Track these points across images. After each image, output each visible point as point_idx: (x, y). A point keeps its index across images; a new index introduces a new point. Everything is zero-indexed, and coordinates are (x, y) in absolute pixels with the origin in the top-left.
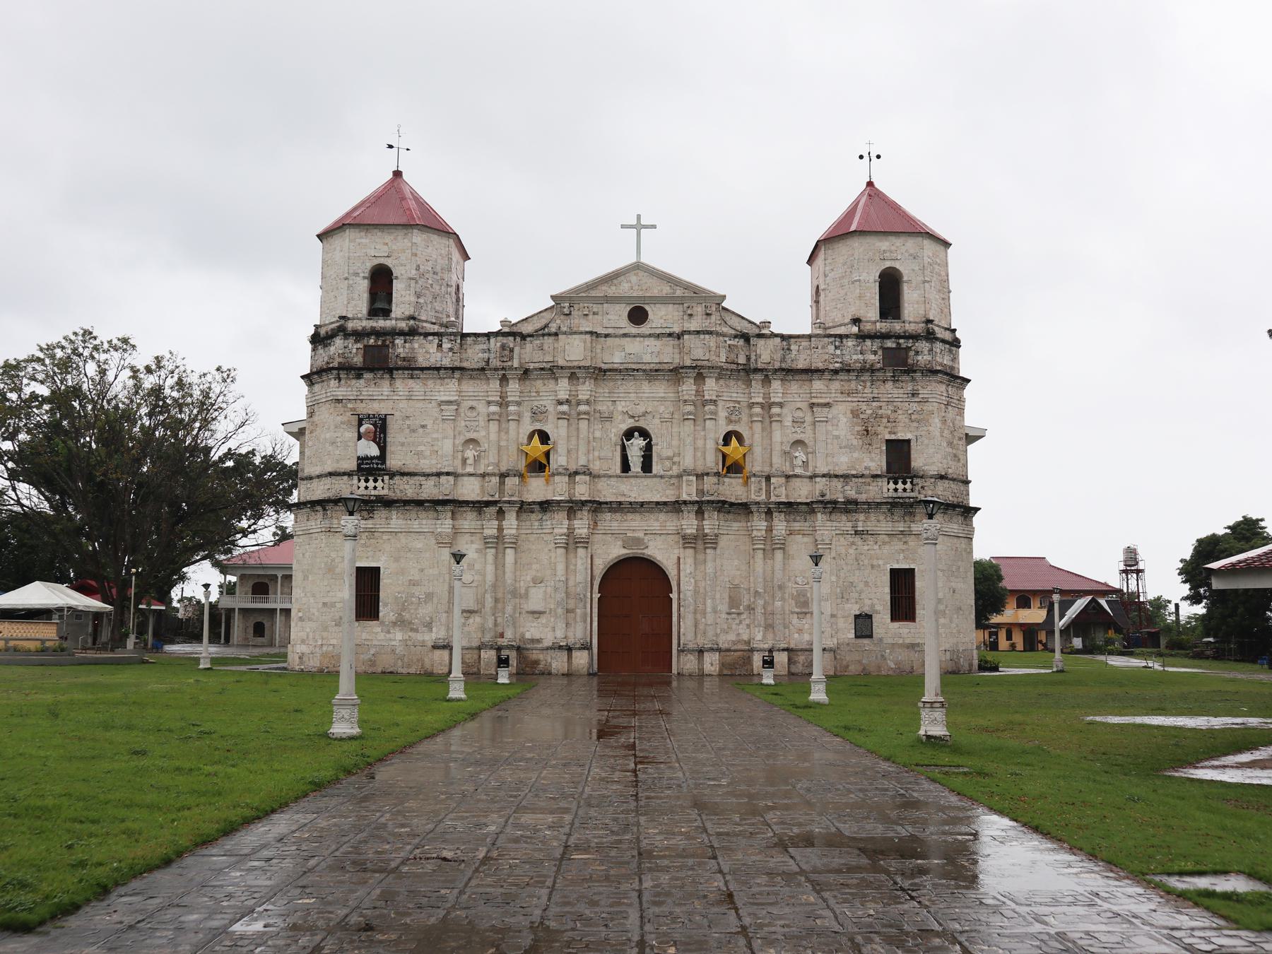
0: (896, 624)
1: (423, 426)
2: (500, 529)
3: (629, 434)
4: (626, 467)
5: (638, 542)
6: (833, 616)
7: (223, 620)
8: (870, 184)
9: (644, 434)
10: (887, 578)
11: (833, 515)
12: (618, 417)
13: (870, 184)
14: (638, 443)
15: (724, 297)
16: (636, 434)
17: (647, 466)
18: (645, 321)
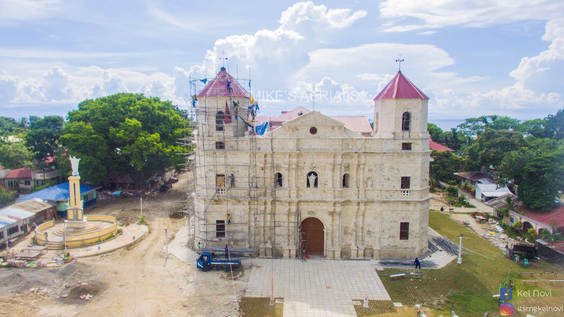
0: (402, 241)
1: (238, 171)
2: (266, 208)
3: (310, 174)
4: (308, 185)
5: (313, 212)
6: (379, 238)
7: (225, 263)
8: (400, 72)
9: (315, 174)
10: (399, 225)
11: (381, 204)
12: (306, 168)
13: (400, 72)
14: (312, 178)
15: (344, 124)
16: (312, 174)
17: (316, 184)
18: (316, 133)
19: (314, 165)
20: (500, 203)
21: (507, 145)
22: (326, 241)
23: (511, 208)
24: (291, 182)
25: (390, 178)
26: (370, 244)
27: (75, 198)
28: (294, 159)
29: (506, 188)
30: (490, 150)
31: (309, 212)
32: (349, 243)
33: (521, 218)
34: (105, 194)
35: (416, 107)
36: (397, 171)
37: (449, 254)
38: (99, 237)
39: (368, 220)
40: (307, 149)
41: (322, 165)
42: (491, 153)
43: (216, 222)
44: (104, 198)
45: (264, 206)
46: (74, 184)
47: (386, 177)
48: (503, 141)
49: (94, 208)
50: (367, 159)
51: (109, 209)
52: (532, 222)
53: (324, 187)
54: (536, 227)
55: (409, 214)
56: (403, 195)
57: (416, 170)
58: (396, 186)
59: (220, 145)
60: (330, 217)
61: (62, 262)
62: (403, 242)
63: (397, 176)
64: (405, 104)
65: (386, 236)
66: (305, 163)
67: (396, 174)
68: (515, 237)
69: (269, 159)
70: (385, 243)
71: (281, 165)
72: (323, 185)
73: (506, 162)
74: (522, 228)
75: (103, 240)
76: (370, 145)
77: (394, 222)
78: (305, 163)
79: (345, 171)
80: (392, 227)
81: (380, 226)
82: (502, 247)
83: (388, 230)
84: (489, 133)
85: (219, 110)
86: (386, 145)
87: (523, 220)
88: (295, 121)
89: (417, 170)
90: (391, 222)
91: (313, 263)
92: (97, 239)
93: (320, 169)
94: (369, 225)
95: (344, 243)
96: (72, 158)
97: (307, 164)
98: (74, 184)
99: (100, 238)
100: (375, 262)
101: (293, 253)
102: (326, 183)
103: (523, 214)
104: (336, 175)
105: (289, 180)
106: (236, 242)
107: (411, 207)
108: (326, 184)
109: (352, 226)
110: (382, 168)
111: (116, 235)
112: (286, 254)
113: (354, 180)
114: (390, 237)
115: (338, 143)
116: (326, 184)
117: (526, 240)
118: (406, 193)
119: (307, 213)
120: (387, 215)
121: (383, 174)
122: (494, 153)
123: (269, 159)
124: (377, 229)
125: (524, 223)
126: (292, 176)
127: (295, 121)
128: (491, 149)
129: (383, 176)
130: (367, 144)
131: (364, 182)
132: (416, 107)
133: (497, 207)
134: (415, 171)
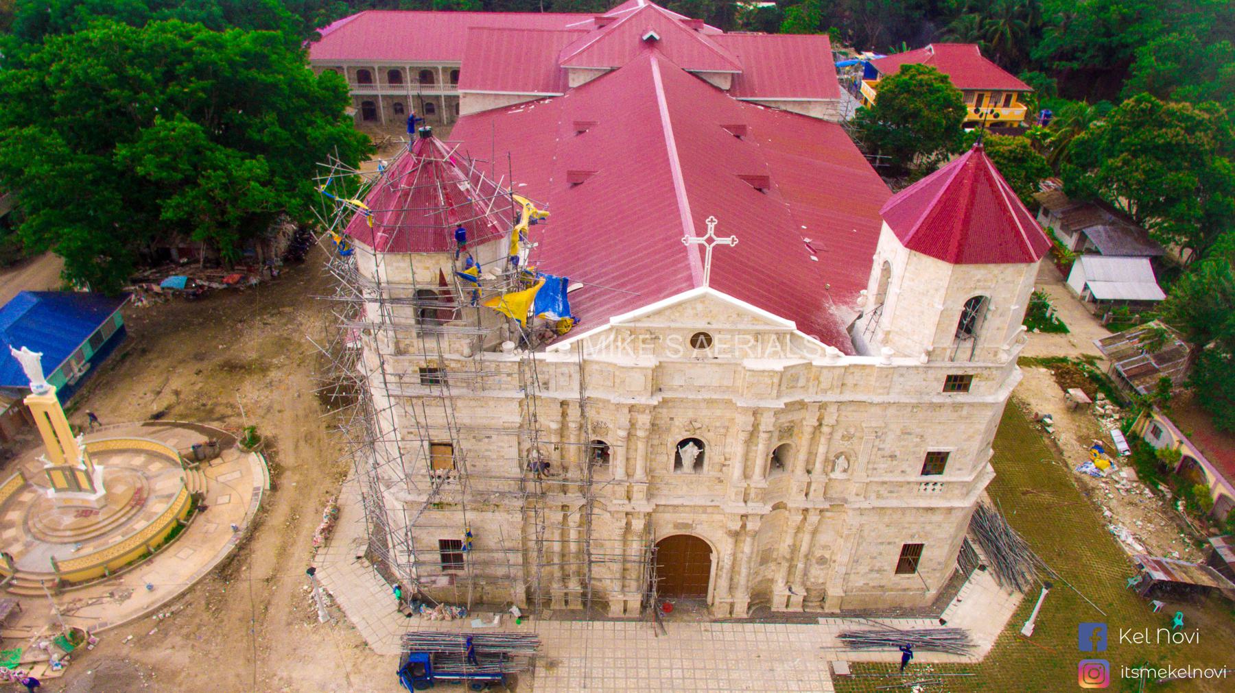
3: (683, 443)
4: (678, 462)
5: (686, 525)
9: (698, 443)
12: (675, 430)
17: (699, 462)
19: (697, 425)
20: (1133, 355)
21: (1183, 154)
22: (716, 581)
23: (1163, 405)
24: (632, 462)
25: (897, 453)
26: (821, 581)
27: (52, 427)
28: (645, 416)
29: (1143, 266)
30: (1134, 161)
31: (676, 526)
32: (770, 577)
33: (1181, 442)
34: (146, 291)
35: (1007, 282)
36: (918, 440)
37: (1001, 585)
38: (146, 543)
39: (824, 538)
40: (682, 386)
41: (718, 424)
42: (1137, 170)
43: (438, 545)
44: (145, 302)
45: (561, 514)
46: (46, 414)
47: (887, 453)
48: (1174, 142)
49: (123, 359)
50: (844, 414)
51: (163, 364)
52: (1207, 467)
53: (721, 470)
54: (1216, 484)
55: (928, 528)
56: (922, 490)
57: (970, 438)
58: (908, 470)
59: (431, 375)
60: (730, 540)
61: (63, 662)
62: (902, 578)
63: (917, 449)
64: (979, 277)
65: (863, 569)
66: (672, 419)
67: (916, 446)
68: (1155, 485)
69: (574, 413)
70: (858, 582)
71: (608, 424)
72: (717, 467)
73: (1183, 291)
74: (1176, 465)
75: (159, 546)
76: (856, 378)
77: (889, 543)
78: (672, 419)
79: (779, 440)
80: (880, 554)
81: (853, 552)
82: (1123, 542)
83: (871, 558)
84: (1143, 111)
85: (419, 287)
86: (902, 379)
87: (1186, 450)
88: (648, 317)
89: (973, 437)
90: (882, 543)
91: (681, 631)
92: (142, 550)
93: (711, 434)
94: (825, 547)
95: (759, 578)
96: (19, 349)
97: (676, 422)
98: (46, 414)
99: (148, 546)
100: (827, 631)
101: (635, 601)
102: (727, 463)
103: (1188, 437)
104: (754, 448)
105: (628, 459)
106: (493, 580)
107: (937, 518)
108: (724, 465)
109: (783, 548)
110: (879, 434)
111: (188, 520)
112: (615, 608)
113: (803, 456)
114: (871, 570)
115: (770, 382)
116: (724, 465)
117: (1179, 503)
118: (930, 487)
119: (671, 526)
120: (874, 531)
121: (881, 446)
122: (1144, 172)
123: (574, 413)
124: (842, 558)
125: (1186, 457)
126: (636, 450)
127: (648, 317)
128: (1139, 160)
129: (879, 449)
130: (851, 376)
131: (826, 460)
132: (1007, 282)
133: (1123, 366)
134: (965, 440)
